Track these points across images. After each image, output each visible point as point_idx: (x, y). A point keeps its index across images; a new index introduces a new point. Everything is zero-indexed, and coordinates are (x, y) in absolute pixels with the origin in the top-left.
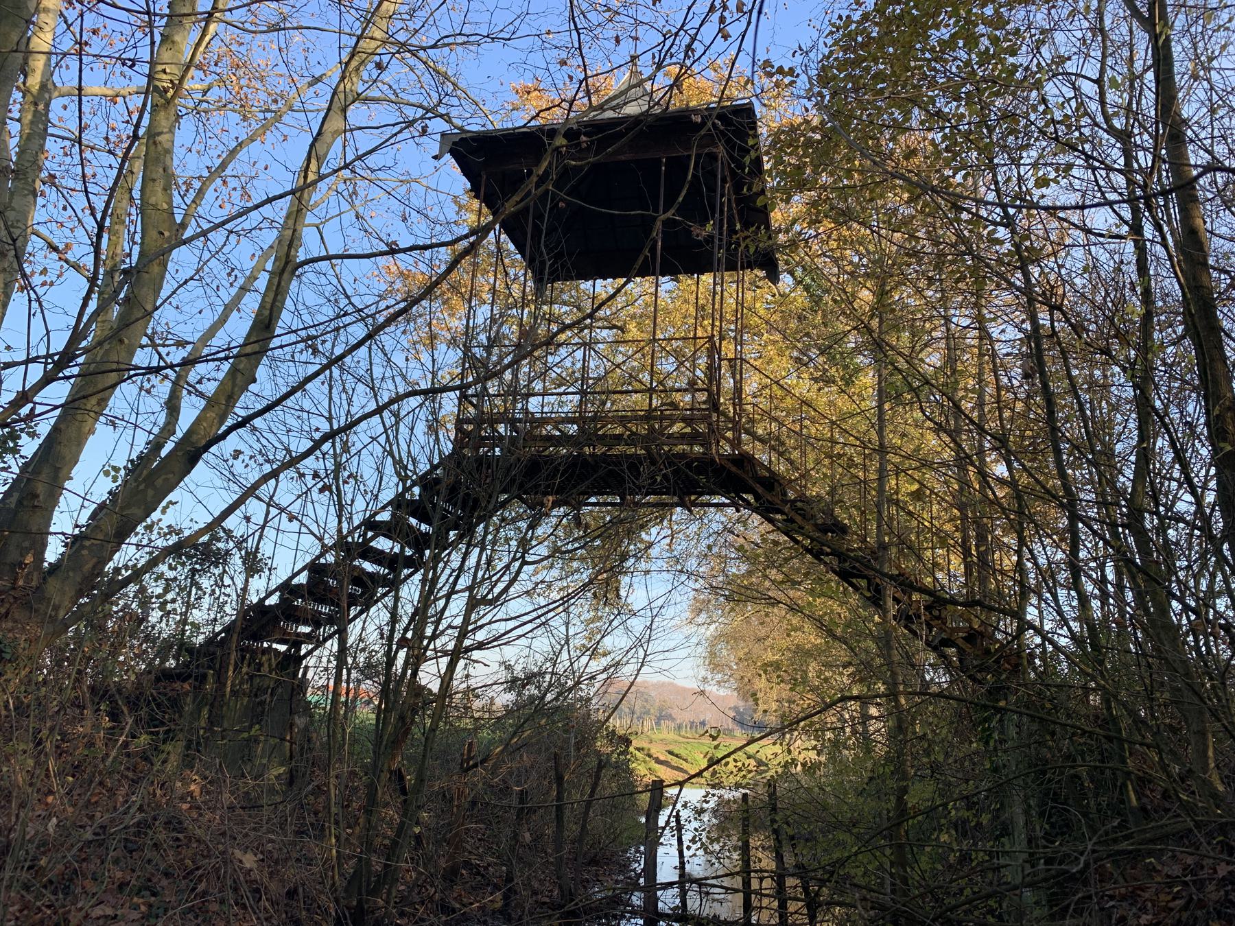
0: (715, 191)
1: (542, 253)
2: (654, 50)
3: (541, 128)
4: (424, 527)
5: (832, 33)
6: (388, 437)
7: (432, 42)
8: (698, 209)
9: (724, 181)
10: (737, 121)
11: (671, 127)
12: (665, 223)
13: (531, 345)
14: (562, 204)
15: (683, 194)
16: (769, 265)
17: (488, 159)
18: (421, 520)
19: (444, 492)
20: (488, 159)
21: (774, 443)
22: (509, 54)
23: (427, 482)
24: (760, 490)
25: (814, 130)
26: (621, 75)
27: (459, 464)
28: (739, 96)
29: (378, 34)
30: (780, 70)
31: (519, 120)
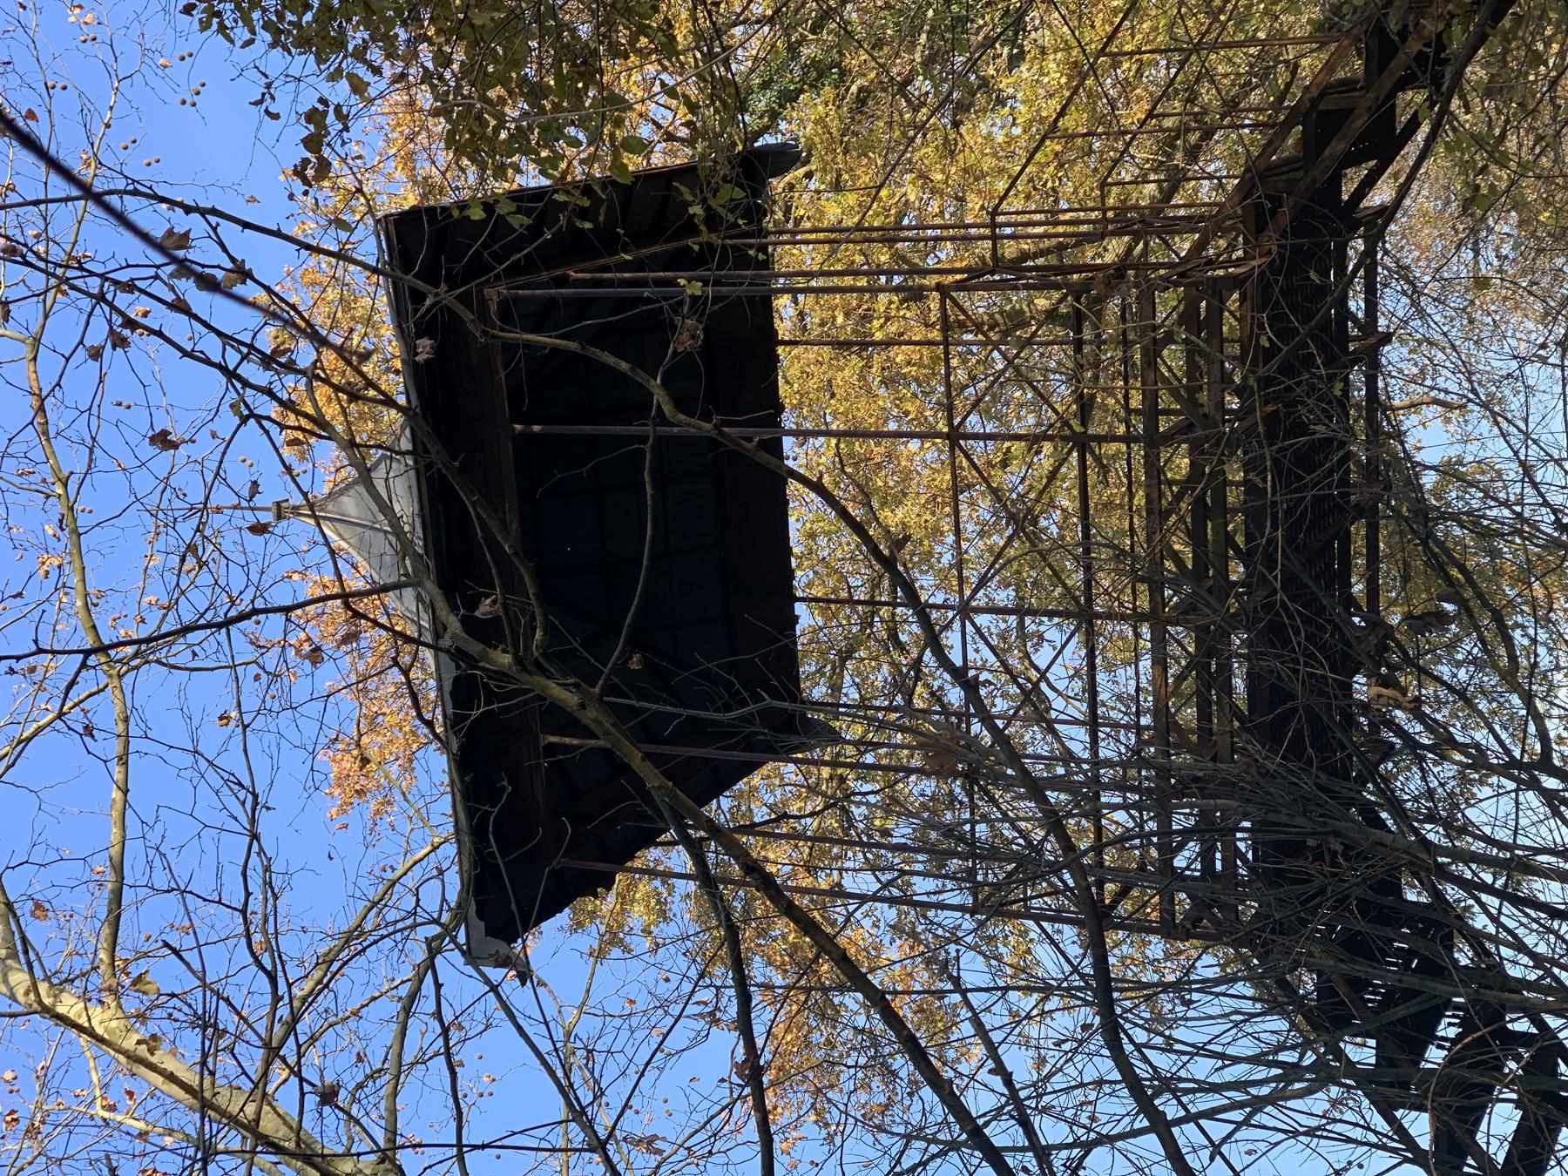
0: (590, 300)
1: (741, 718)
2: (279, 439)
3: (453, 723)
4: (1448, 1029)
5: (222, 28)
6: (1211, 1114)
7: (263, 982)
8: (643, 331)
9: (563, 282)
10: (423, 247)
11: (447, 400)
12: (681, 404)
13: (966, 755)
14: (635, 664)
15: (611, 360)
16: (761, 165)
17: (535, 842)
18: (1431, 1038)
19: (1360, 969)
20: (535, 842)
21: (1183, 143)
22: (283, 796)
23: (1328, 1019)
24: (1337, 147)
25: (444, 60)
26: (327, 520)
27: (1280, 929)
28: (368, 247)
29: (250, 1109)
30: (313, 143)
31: (436, 765)
